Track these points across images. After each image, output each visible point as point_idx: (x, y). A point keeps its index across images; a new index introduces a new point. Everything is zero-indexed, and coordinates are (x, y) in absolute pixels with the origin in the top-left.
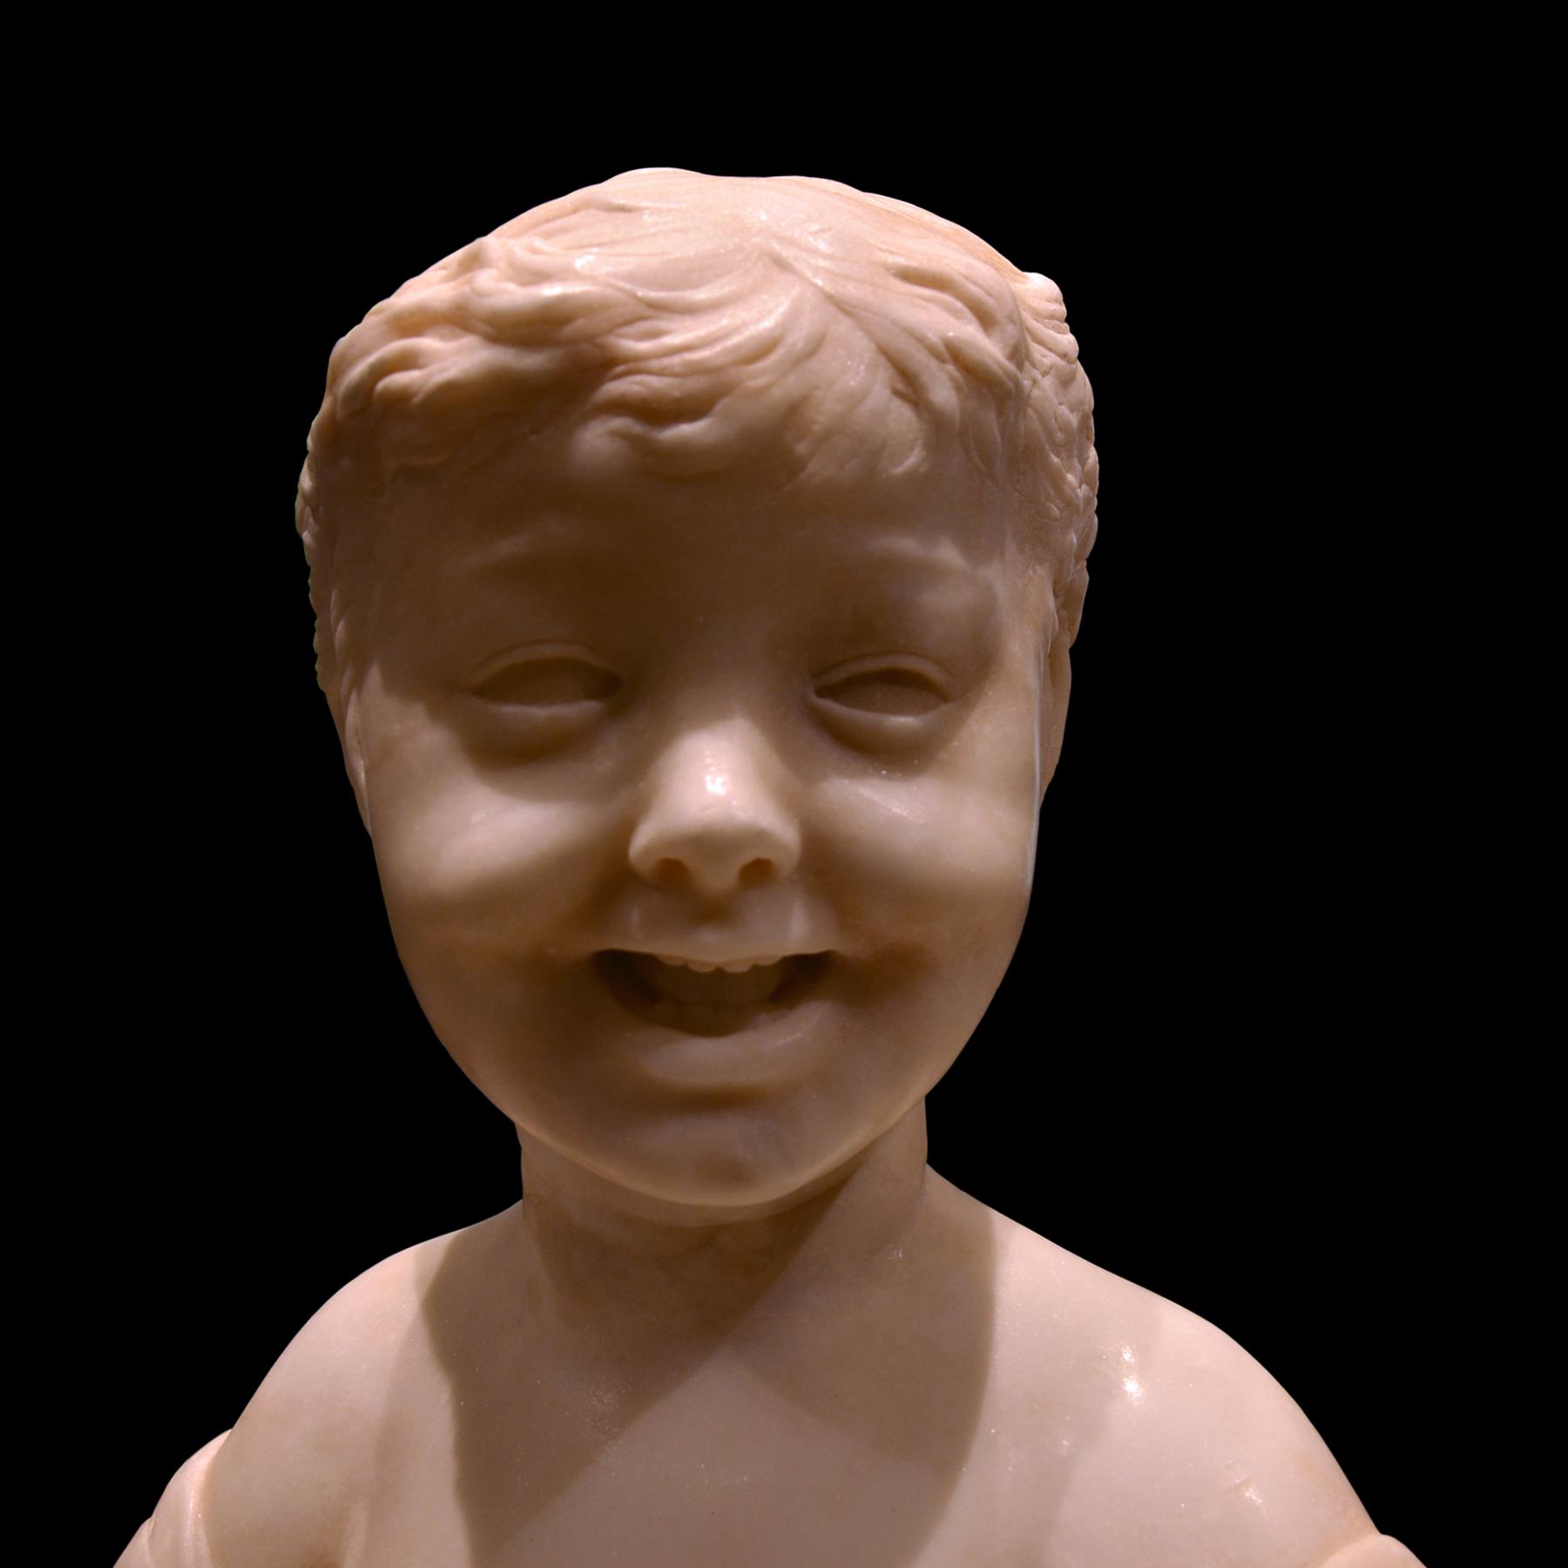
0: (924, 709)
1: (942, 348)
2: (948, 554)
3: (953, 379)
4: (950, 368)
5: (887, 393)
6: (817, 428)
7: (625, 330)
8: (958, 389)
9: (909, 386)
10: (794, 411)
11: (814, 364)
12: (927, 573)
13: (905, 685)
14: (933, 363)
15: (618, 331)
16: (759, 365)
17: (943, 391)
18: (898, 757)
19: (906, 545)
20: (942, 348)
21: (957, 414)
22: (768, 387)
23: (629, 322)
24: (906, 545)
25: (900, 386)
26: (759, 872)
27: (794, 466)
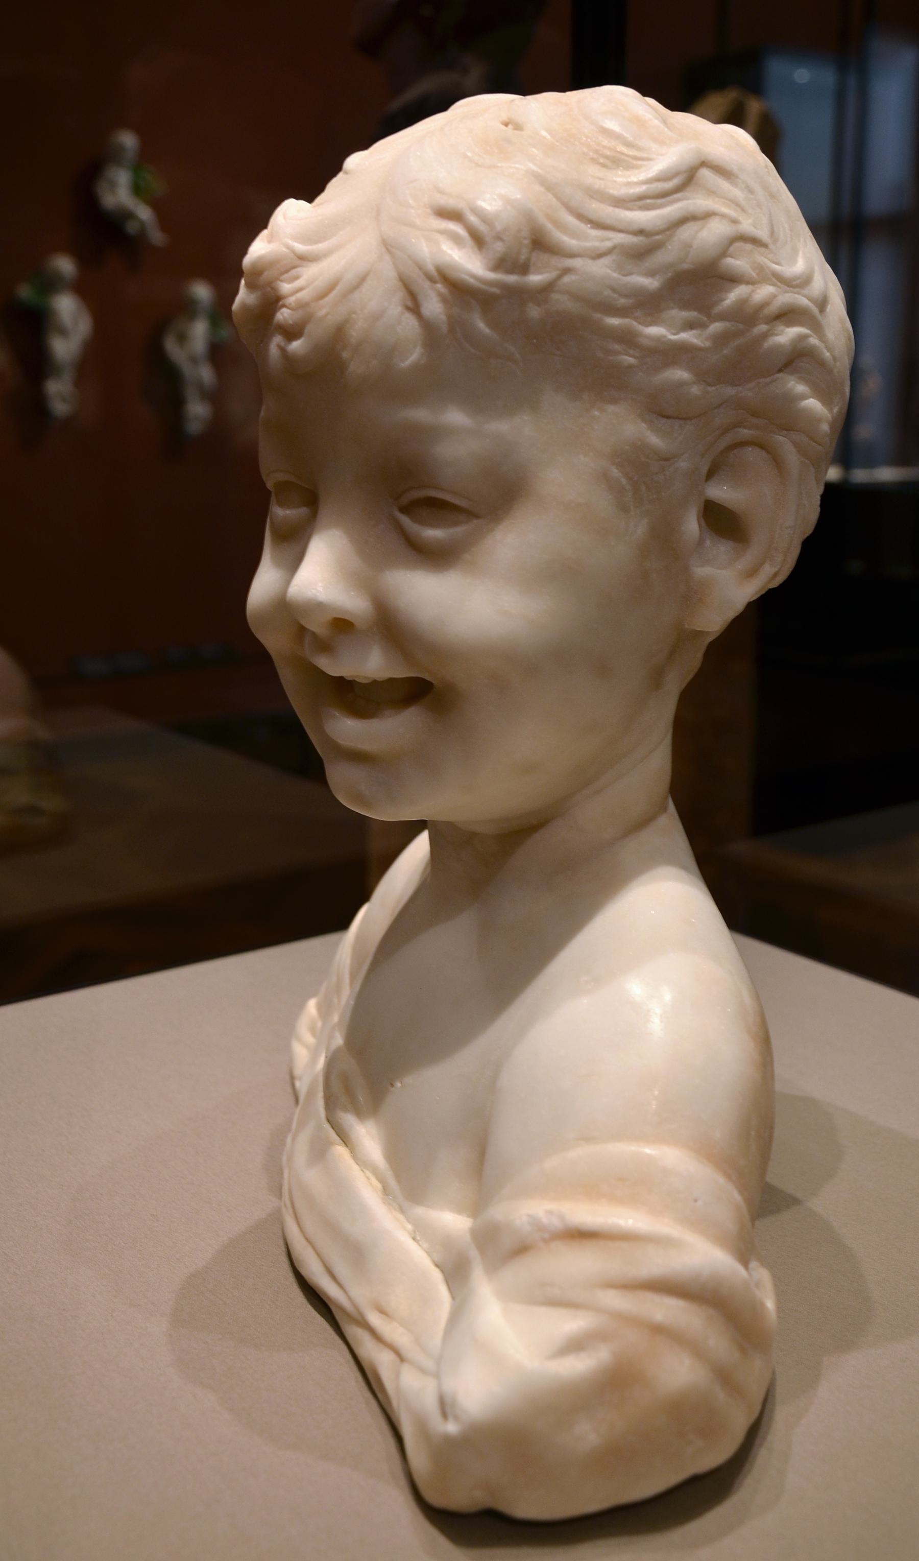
0: (456, 524)
1: (434, 273)
2: (456, 417)
3: (440, 294)
4: (439, 286)
5: (400, 309)
6: (353, 341)
7: (286, 276)
8: (444, 300)
9: (414, 306)
10: (339, 333)
11: (357, 295)
12: (435, 433)
13: (437, 508)
14: (427, 284)
15: (282, 277)
16: (327, 299)
17: (433, 307)
18: (436, 557)
19: (420, 415)
20: (434, 273)
21: (443, 317)
22: (327, 314)
23: (287, 271)
24: (420, 415)
25: (409, 303)
26: (342, 625)
27: (341, 366)
